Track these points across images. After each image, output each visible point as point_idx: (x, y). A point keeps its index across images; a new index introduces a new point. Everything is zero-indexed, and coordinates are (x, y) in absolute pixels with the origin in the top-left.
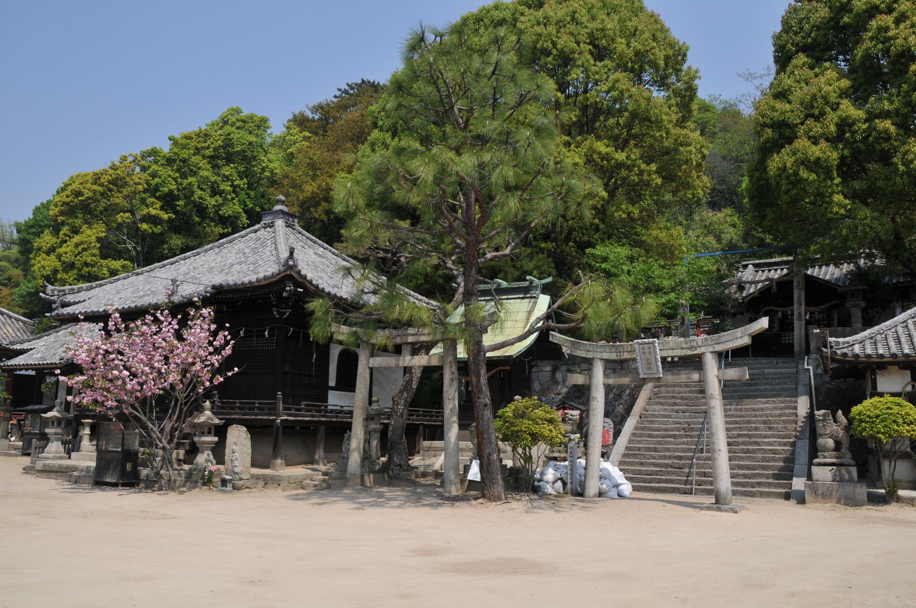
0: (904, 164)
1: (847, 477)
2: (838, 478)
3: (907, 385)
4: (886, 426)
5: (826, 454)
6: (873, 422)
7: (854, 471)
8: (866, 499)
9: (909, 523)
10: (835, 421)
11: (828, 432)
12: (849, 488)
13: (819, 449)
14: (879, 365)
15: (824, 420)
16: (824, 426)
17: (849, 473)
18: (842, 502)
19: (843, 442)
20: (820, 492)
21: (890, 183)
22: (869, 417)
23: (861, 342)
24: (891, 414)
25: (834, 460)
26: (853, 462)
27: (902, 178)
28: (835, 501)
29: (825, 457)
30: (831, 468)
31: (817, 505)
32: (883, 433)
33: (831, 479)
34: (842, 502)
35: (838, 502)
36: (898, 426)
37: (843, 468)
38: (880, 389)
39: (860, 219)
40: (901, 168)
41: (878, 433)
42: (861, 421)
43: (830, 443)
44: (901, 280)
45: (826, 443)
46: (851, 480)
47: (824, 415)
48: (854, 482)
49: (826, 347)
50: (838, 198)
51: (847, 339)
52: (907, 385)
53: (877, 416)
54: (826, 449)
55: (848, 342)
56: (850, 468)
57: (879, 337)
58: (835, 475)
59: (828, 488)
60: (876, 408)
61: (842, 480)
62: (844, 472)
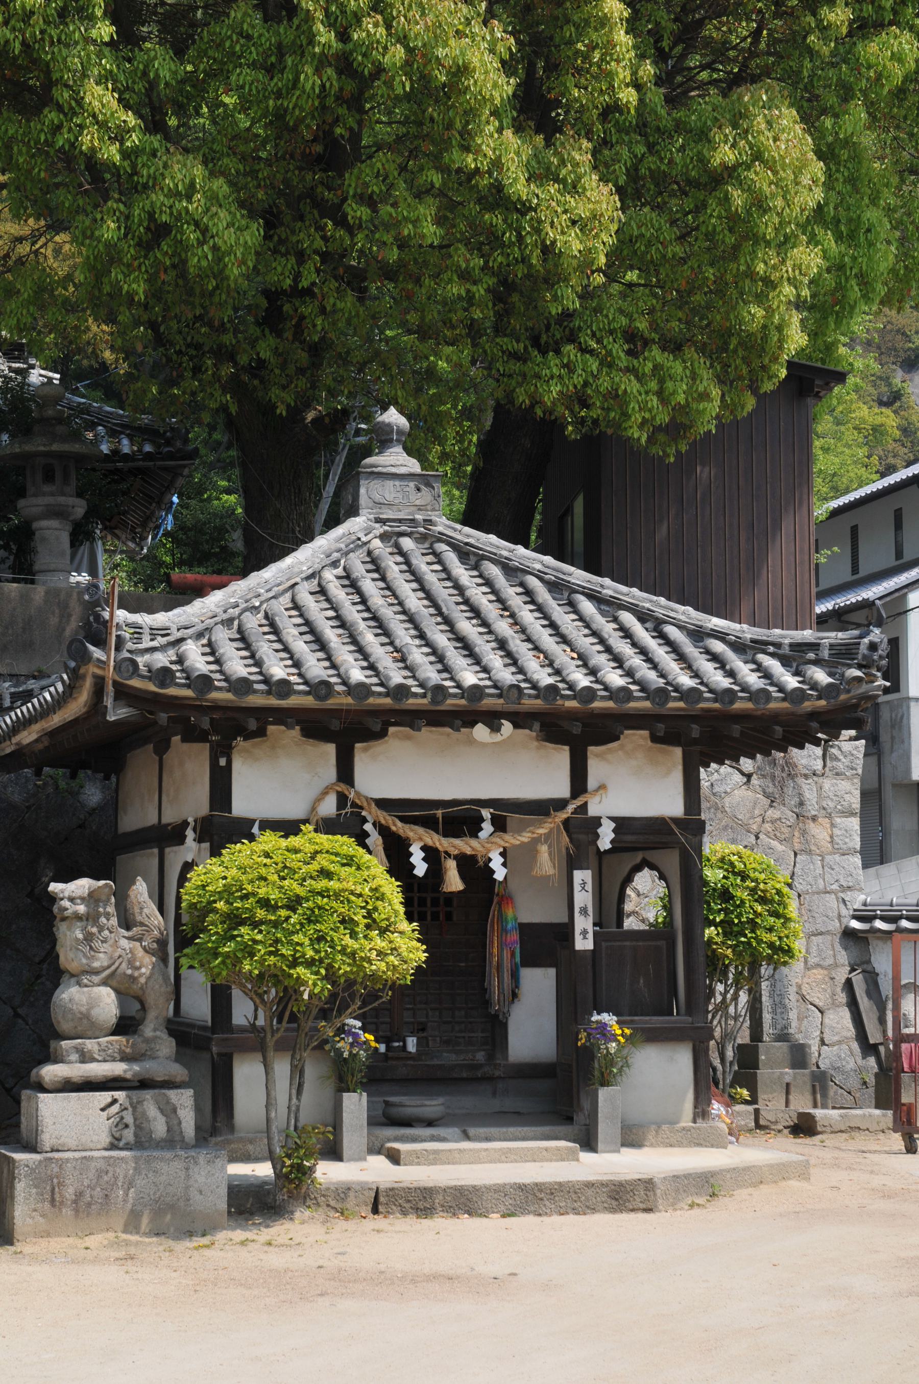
0: (331, 22)
1: (159, 1127)
2: (129, 1135)
3: (325, 793)
4: (321, 939)
5: (90, 1045)
6: (276, 924)
7: (184, 1101)
8: (223, 1205)
9: (414, 1280)
10: (127, 922)
11: (101, 961)
12: (169, 1169)
13: (65, 1026)
14: (227, 723)
15: (91, 918)
16: (89, 938)
17: (169, 1111)
18: (145, 1221)
19: (150, 999)
20: (69, 1193)
21: (277, 83)
22: (265, 903)
23: (199, 635)
24: (337, 895)
25: (118, 1068)
26: (178, 1071)
27: (318, 71)
28: (119, 1221)
29: (85, 1057)
30: (105, 1097)
31: (57, 1244)
32: (310, 964)
33: (105, 1139)
34: (145, 1221)
35: (132, 1224)
36: (353, 935)
37: (148, 1095)
38: (243, 804)
39: (175, 194)
40: (325, 36)
41: (294, 964)
42: (235, 920)
43: (106, 1004)
44: (126, 446)
45: (93, 1003)
46: (173, 1141)
47: (92, 898)
48: (186, 1146)
49: (101, 643)
50: (100, 97)
51: (160, 619)
52: (325, 793)
53: (293, 904)
54: (87, 1027)
55: (164, 631)
56: (172, 1094)
57: (253, 622)
58: (122, 1124)
59: (100, 1173)
60: (286, 872)
61: (143, 1142)
62: (152, 1110)
